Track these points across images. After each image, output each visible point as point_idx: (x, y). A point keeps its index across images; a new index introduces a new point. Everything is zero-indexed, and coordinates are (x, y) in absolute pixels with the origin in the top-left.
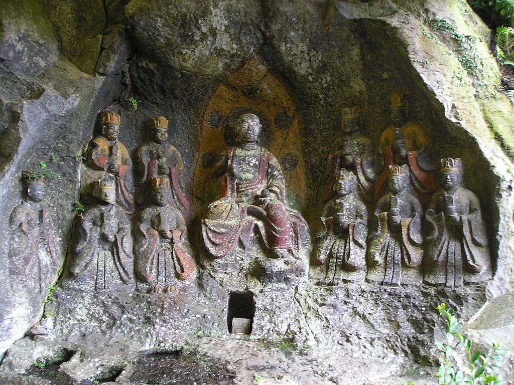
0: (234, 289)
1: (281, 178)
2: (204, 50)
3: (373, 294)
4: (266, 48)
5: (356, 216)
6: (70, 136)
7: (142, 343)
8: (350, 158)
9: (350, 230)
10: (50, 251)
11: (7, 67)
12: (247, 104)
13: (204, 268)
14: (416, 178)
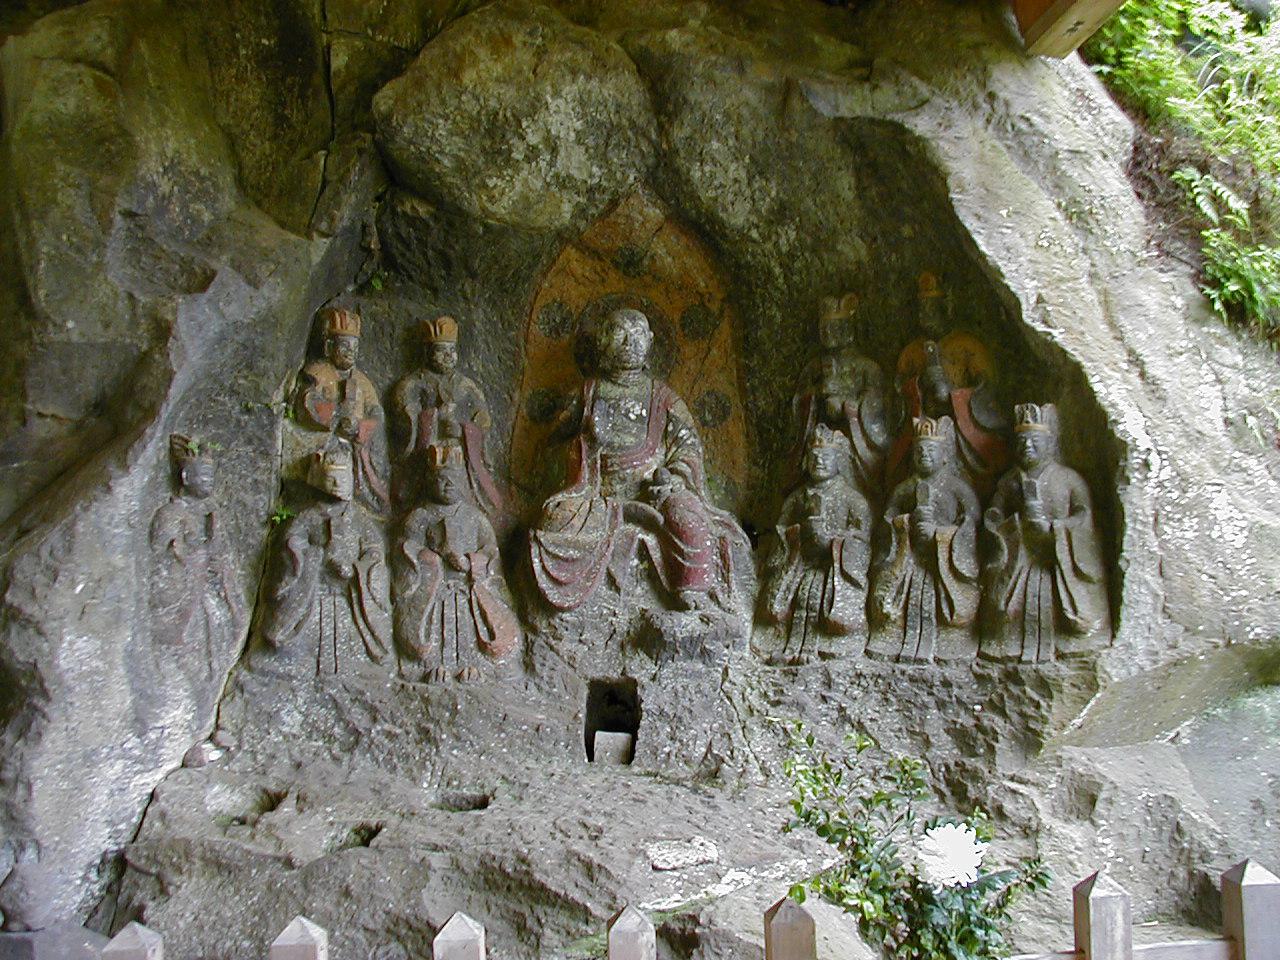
0: (598, 675)
1: (693, 444)
2: (528, 180)
3: (880, 681)
4: (661, 174)
5: (848, 523)
6: (262, 363)
7: (414, 779)
8: (836, 403)
9: (836, 553)
10: (226, 597)
11: (142, 228)
13: (535, 630)
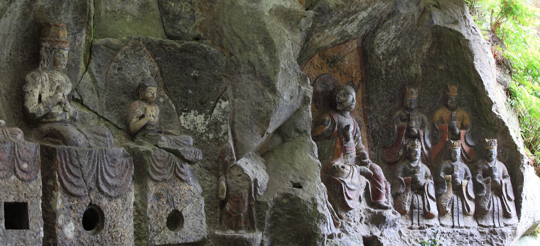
14: (464, 150)
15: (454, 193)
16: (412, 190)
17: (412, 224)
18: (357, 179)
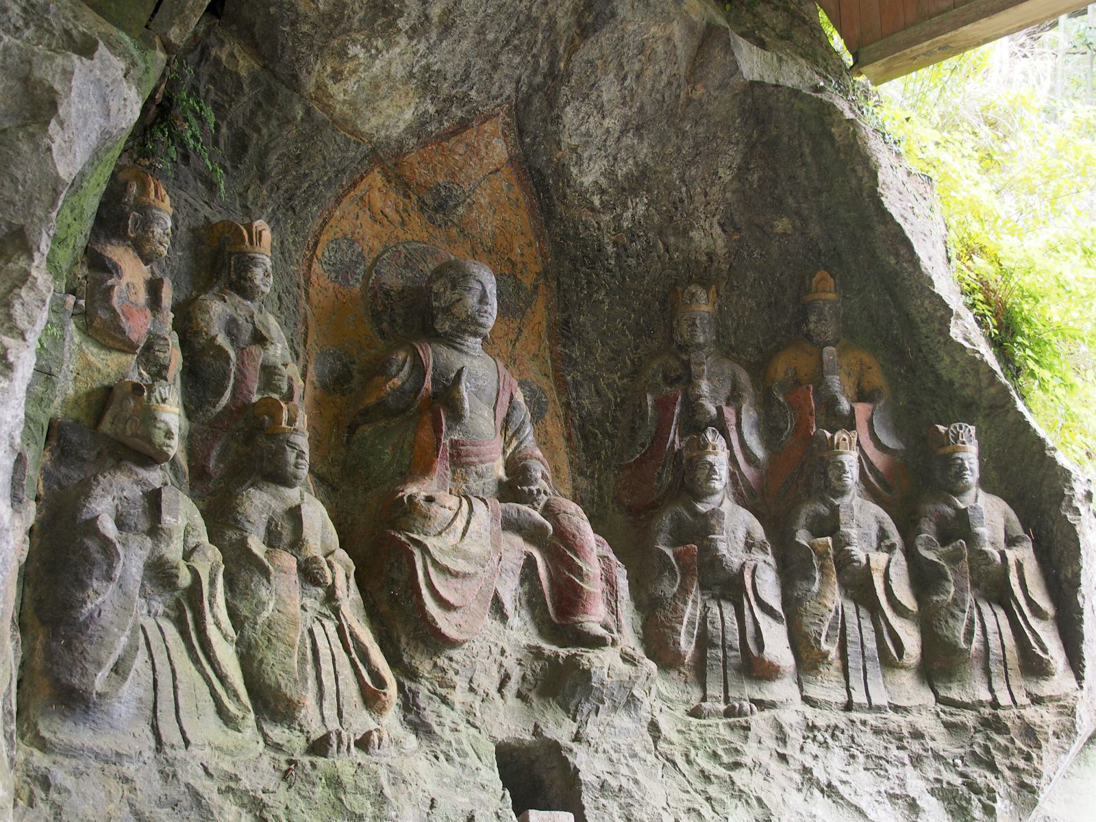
12: (425, 234)
13: (413, 675)
14: (870, 464)
15: (847, 596)
16: (703, 587)
17: (704, 699)
18: (486, 541)
